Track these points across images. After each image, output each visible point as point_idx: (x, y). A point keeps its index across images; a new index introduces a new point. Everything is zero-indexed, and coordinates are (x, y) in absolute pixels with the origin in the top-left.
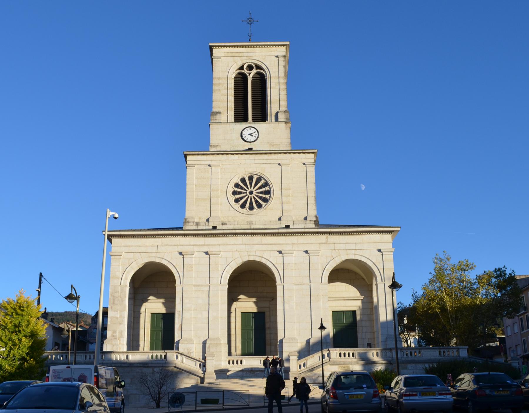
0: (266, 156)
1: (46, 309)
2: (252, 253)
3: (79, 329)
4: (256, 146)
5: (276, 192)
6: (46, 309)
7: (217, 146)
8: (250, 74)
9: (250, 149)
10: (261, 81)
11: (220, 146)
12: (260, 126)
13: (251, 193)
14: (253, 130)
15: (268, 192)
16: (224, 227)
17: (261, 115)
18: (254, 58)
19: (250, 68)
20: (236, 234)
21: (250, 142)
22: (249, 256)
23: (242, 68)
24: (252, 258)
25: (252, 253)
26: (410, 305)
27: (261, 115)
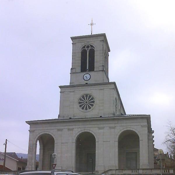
0: (93, 86)
1: (90, 54)
2: (86, 129)
3: (170, 156)
4: (88, 82)
5: (96, 101)
6: (90, 54)
7: (73, 83)
8: (88, 50)
9: (87, 83)
10: (92, 52)
11: (74, 83)
12: (92, 73)
13: (86, 102)
14: (88, 76)
15: (87, 96)
16: (75, 118)
17: (92, 69)
18: (90, 42)
19: (88, 47)
20: (79, 121)
21: (89, 80)
22: (84, 130)
23: (84, 47)
24: (86, 131)
25: (86, 129)
26: (22, 157)
27: (92, 69)
